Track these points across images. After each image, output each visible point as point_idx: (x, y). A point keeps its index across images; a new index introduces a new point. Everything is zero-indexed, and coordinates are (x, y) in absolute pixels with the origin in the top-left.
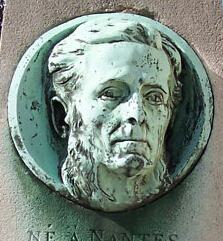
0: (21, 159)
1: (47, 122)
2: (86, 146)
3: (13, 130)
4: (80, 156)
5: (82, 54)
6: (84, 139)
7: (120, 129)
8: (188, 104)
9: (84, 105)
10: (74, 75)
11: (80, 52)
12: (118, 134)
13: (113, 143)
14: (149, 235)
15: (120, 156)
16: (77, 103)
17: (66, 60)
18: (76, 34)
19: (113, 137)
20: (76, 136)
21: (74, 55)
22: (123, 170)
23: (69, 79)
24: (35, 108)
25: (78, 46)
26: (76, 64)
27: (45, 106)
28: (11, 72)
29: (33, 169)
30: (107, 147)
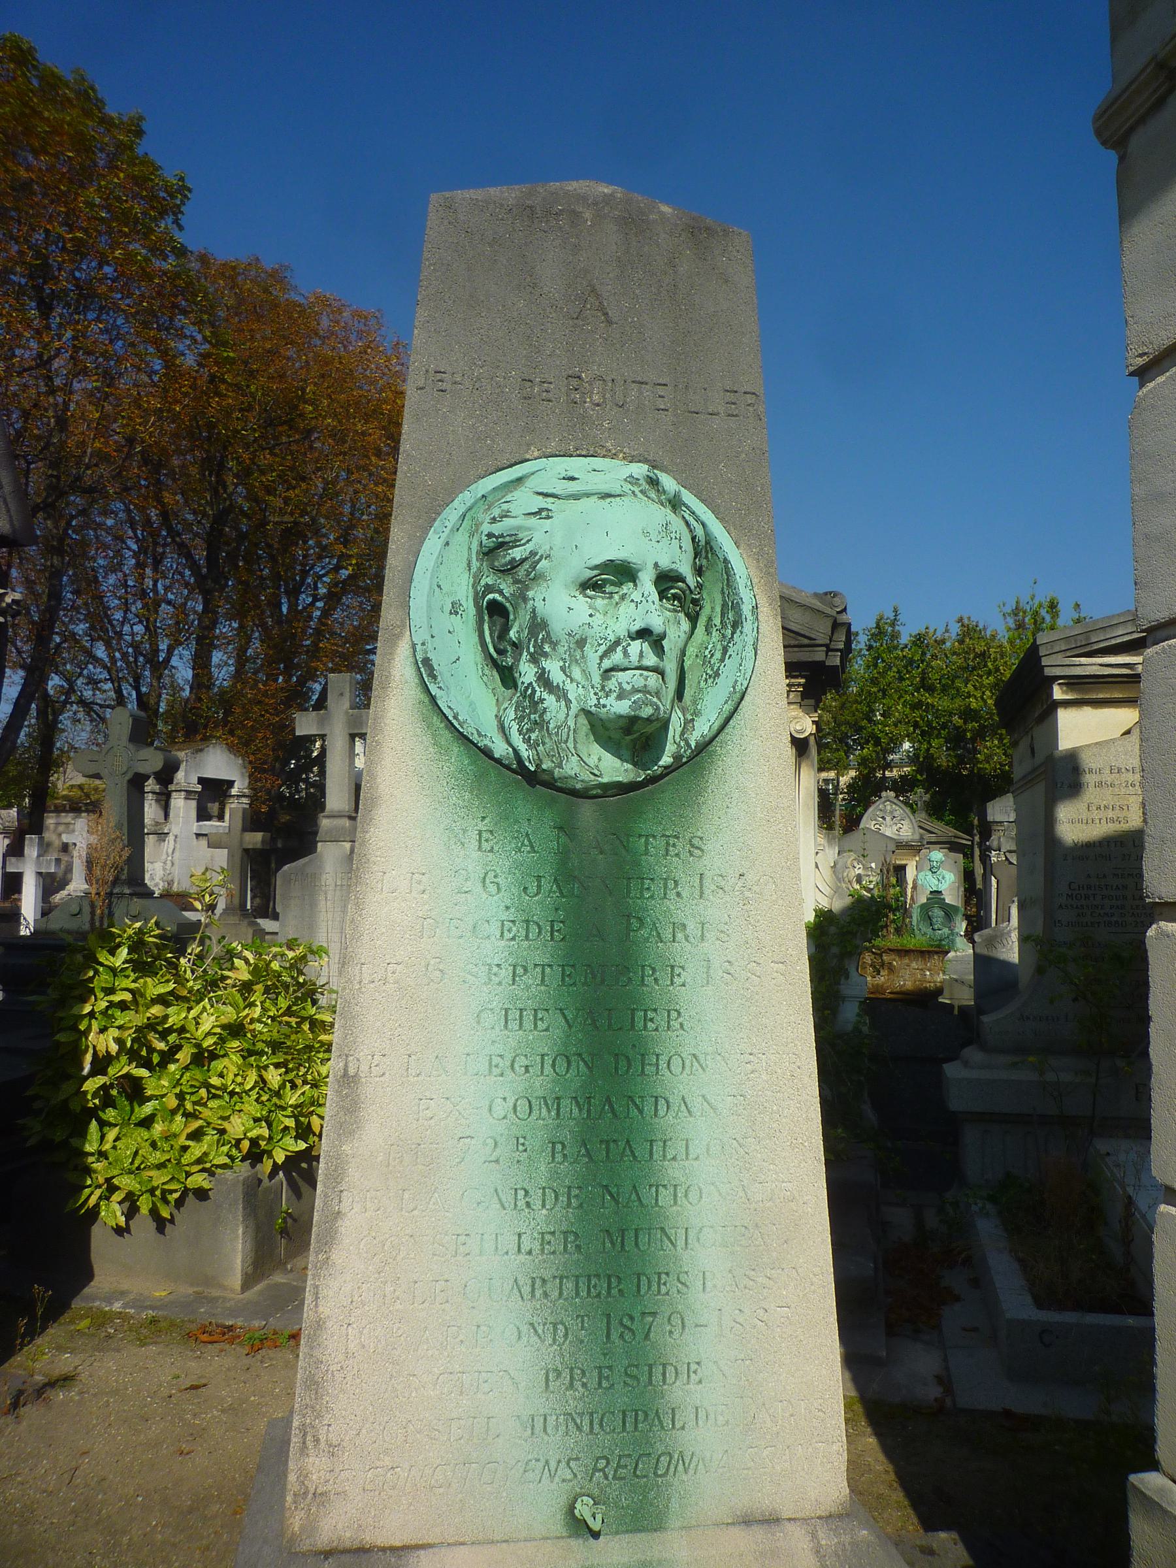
0: (433, 699)
1: (476, 639)
2: (557, 677)
3: (418, 647)
4: (545, 695)
5: (548, 517)
6: (553, 667)
7: (619, 649)
8: (710, 619)
9: (560, 604)
10: (533, 553)
11: (544, 514)
12: (617, 657)
13: (607, 673)
14: (654, 837)
15: (620, 697)
16: (539, 604)
17: (519, 528)
18: (531, 483)
19: (607, 663)
20: (534, 659)
21: (533, 521)
22: (621, 723)
23: (523, 561)
24: (456, 613)
25: (541, 502)
26: (538, 537)
27: (472, 611)
28: (493, 469)
29: (455, 717)
30: (597, 679)
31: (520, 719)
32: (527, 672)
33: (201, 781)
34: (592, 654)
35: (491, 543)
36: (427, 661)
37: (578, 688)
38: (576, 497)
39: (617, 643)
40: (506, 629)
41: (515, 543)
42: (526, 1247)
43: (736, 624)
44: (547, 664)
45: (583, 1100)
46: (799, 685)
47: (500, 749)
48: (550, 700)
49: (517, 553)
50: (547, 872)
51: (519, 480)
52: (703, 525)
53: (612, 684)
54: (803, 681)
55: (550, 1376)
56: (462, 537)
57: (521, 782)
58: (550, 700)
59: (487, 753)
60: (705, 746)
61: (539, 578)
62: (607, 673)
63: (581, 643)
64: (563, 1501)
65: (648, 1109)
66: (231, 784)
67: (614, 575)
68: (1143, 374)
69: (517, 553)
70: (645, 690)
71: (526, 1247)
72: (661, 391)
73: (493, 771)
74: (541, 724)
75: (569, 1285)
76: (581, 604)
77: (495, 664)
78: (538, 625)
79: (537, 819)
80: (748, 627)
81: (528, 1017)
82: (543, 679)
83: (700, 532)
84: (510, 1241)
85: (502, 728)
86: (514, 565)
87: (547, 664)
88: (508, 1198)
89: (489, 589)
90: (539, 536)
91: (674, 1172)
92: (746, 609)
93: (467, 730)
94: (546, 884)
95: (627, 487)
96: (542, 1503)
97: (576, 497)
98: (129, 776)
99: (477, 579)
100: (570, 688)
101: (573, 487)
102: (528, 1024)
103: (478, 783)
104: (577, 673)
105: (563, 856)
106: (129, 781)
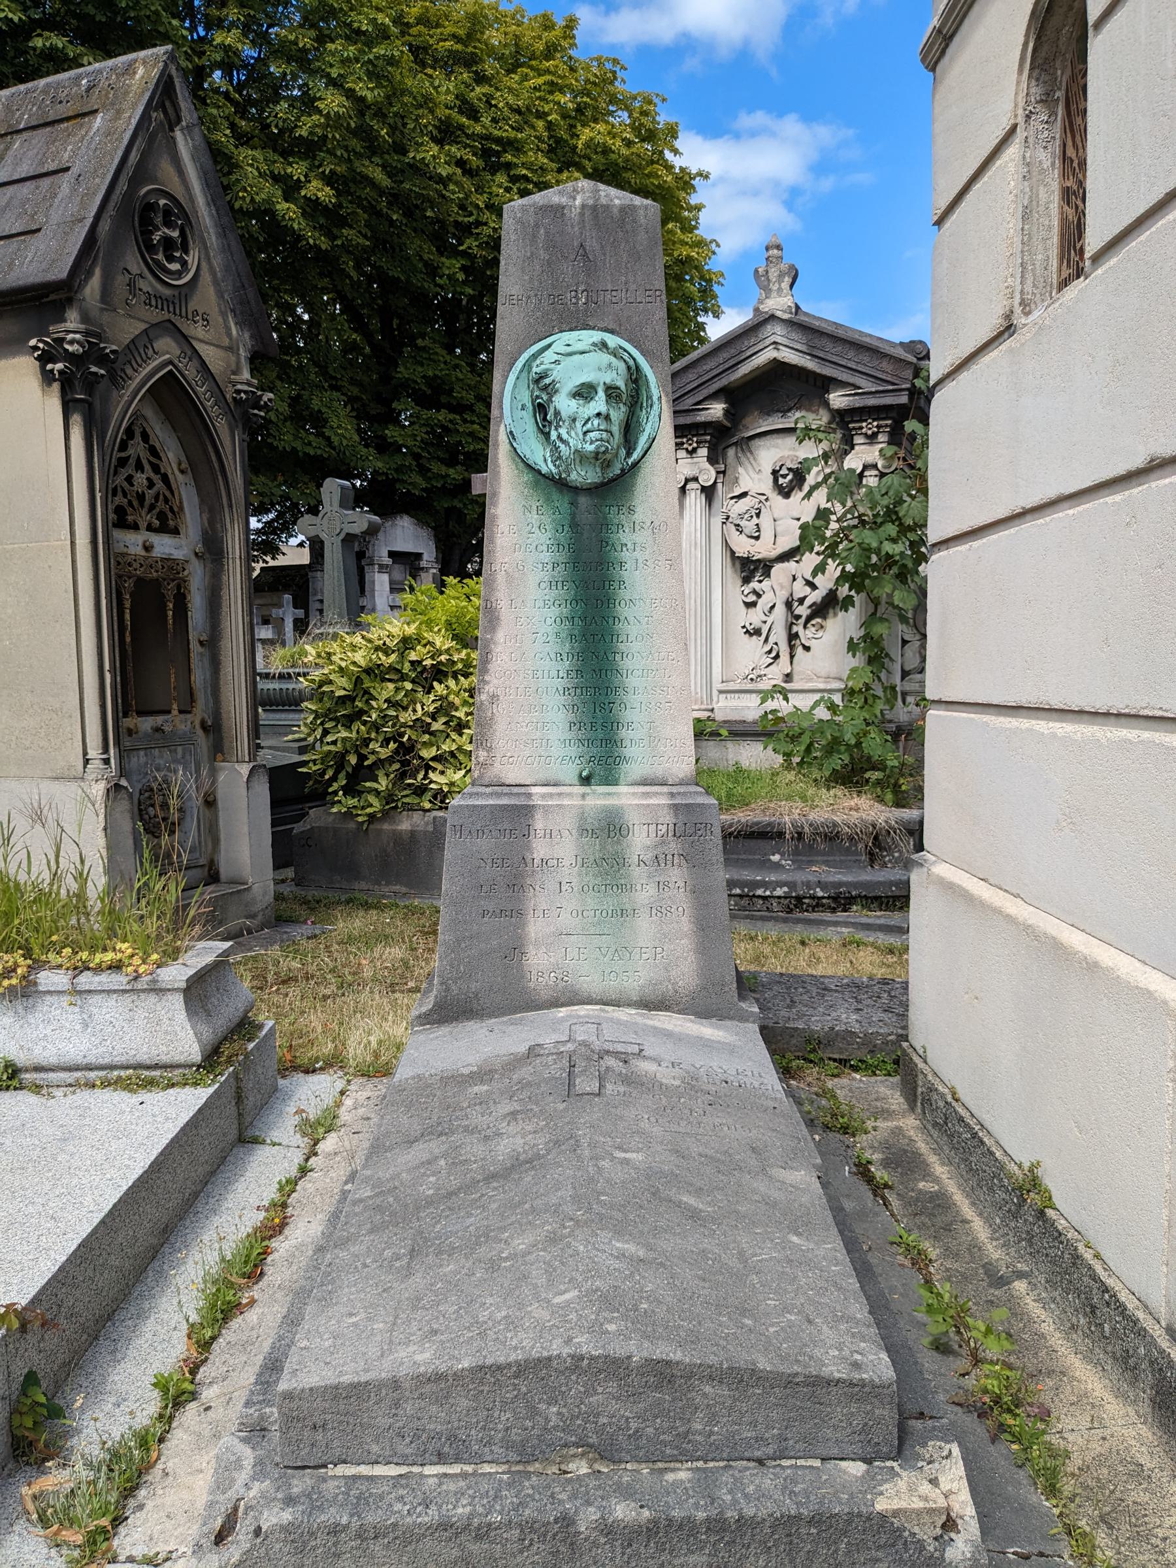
2: (565, 436)
6: (563, 431)
9: (564, 404)
12: (589, 426)
13: (585, 433)
19: (585, 429)
20: (556, 429)
25: (556, 357)
27: (531, 408)
30: (581, 436)
31: (551, 456)
32: (554, 435)
33: (392, 554)
34: (578, 424)
35: (536, 377)
36: (511, 432)
37: (574, 440)
38: (570, 354)
39: (589, 419)
40: (546, 415)
41: (546, 376)
42: (561, 675)
43: (651, 406)
44: (561, 431)
45: (584, 618)
46: (886, 426)
47: (544, 470)
48: (562, 447)
49: (547, 381)
50: (566, 523)
51: (549, 346)
52: (634, 359)
53: (588, 438)
54: (889, 422)
55: (572, 724)
56: (524, 374)
57: (552, 485)
58: (562, 447)
59: (539, 472)
60: (636, 464)
61: (556, 391)
62: (585, 433)
63: (574, 420)
64: (577, 772)
65: (611, 621)
66: (419, 556)
67: (584, 392)
68: (939, 222)
69: (547, 381)
70: (601, 440)
71: (561, 675)
72: (614, 293)
73: (542, 480)
74: (560, 458)
75: (579, 691)
76: (573, 403)
77: (542, 432)
78: (557, 413)
79: (562, 502)
80: (656, 407)
81: (560, 584)
82: (559, 437)
83: (631, 363)
84: (554, 673)
85: (545, 460)
86: (546, 387)
87: (561, 431)
88: (553, 656)
89: (538, 397)
90: (557, 373)
91: (622, 647)
92: (655, 398)
93: (530, 462)
94: (566, 528)
95: (592, 348)
96: (570, 771)
97: (570, 354)
98: (342, 536)
99: (532, 392)
100: (571, 440)
101: (569, 349)
102: (560, 587)
103: (536, 484)
104: (573, 434)
105: (573, 516)
106: (343, 541)
